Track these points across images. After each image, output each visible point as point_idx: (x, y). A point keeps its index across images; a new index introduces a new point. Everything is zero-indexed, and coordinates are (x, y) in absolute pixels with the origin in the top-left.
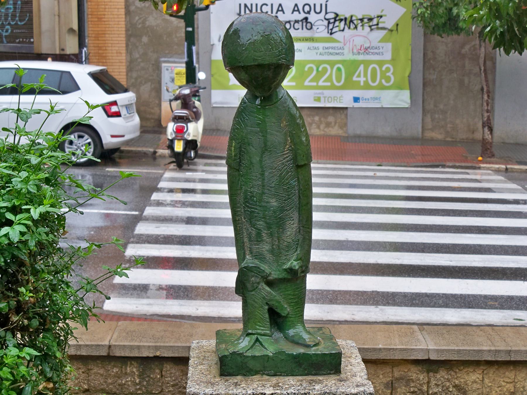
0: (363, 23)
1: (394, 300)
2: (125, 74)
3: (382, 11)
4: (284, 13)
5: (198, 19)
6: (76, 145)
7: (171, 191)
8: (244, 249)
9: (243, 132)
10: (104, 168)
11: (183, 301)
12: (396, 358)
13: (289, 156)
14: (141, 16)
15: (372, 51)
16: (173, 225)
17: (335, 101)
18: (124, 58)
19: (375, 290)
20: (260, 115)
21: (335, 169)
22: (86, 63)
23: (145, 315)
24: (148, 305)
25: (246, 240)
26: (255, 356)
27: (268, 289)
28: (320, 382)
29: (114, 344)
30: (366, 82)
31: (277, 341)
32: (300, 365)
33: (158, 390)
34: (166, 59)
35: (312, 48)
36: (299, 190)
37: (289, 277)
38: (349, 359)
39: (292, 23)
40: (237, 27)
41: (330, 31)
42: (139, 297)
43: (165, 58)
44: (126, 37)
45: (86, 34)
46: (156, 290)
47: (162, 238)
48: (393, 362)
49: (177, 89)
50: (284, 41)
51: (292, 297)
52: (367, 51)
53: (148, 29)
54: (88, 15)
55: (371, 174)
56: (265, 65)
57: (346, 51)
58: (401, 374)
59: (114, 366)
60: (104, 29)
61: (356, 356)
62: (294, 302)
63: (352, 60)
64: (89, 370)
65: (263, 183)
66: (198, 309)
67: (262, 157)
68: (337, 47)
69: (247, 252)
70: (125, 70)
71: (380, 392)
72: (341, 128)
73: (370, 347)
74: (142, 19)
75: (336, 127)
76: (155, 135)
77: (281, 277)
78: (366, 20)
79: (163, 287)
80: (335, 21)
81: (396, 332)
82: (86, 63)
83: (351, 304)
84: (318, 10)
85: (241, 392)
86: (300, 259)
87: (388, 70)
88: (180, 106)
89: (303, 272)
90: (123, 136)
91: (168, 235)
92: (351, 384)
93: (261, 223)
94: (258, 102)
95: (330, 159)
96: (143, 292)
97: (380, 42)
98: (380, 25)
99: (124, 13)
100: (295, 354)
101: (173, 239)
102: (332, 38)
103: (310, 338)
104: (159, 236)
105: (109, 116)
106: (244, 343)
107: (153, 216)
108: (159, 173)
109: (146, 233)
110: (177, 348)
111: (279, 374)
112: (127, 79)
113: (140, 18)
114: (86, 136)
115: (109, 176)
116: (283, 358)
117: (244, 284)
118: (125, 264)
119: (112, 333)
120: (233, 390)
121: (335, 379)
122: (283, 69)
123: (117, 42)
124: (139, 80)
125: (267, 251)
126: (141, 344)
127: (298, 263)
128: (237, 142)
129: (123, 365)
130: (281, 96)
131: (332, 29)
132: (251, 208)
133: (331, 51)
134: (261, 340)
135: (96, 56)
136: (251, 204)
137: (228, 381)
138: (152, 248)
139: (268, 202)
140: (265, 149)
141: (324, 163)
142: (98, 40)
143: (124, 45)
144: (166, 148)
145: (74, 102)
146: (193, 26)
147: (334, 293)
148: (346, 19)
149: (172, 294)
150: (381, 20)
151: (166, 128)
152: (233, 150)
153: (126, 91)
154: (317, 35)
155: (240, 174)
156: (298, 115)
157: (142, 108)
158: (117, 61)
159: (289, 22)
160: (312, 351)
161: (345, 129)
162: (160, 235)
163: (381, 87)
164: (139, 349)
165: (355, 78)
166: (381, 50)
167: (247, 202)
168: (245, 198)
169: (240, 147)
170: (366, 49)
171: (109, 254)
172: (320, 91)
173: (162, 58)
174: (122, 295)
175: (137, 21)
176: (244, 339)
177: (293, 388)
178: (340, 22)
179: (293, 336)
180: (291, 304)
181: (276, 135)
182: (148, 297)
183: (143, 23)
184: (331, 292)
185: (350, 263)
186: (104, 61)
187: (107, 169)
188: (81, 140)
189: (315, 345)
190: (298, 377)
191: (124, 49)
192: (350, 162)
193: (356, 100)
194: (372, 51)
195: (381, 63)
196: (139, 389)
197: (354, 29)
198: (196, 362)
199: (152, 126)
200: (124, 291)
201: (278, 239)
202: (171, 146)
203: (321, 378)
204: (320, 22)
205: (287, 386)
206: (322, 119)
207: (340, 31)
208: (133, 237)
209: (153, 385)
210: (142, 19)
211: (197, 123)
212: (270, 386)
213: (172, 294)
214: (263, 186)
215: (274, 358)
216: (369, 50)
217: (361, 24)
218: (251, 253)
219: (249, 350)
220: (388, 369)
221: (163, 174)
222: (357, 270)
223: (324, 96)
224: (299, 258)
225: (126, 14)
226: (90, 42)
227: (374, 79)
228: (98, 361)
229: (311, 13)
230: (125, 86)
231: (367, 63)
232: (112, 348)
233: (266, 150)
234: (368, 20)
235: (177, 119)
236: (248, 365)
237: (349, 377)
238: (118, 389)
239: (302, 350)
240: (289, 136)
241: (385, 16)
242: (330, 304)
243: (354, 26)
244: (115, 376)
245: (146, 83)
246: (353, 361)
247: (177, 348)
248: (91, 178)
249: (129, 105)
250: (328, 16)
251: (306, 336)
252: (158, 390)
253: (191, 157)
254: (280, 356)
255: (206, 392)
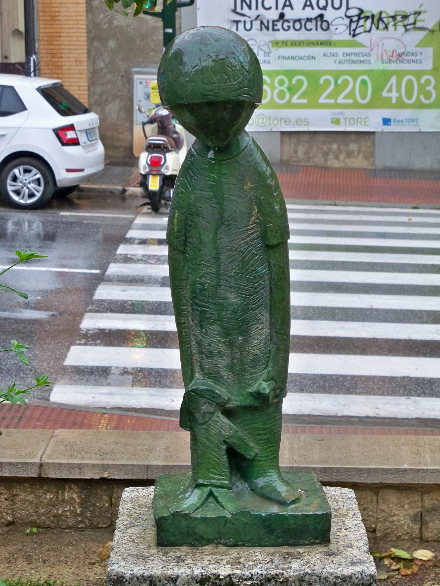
0: (396, 21)
1: (432, 389)
2: (86, 88)
3: (421, 5)
4: (292, 8)
5: (180, 17)
6: (21, 182)
7: (143, 242)
8: (192, 364)
9: (190, 199)
10: (58, 212)
11: (154, 389)
12: (427, 482)
13: (255, 232)
14: (106, 14)
15: (407, 58)
16: (144, 288)
17: (359, 123)
18: (85, 68)
19: (406, 375)
20: (213, 173)
21: (357, 213)
22: (35, 75)
23: (104, 408)
24: (108, 394)
25: (194, 351)
26: (206, 518)
27: (225, 420)
28: (300, 556)
29: (47, 461)
30: (399, 99)
31: (239, 495)
32: (271, 531)
33: (106, 523)
34: (139, 69)
35: (329, 55)
36: (271, 280)
37: (257, 404)
38: (344, 519)
39: (303, 22)
40: (178, 47)
41: (352, 33)
42: (97, 384)
43: (138, 67)
44: (87, 41)
45: (36, 38)
46: (119, 374)
47: (129, 305)
48: (422, 488)
49: (154, 109)
50: (247, 68)
51: (262, 432)
52: (400, 59)
53: (116, 30)
54: (38, 12)
55: (405, 219)
56: (219, 102)
57: (373, 58)
58: (434, 504)
59: (48, 491)
60: (59, 30)
61: (354, 515)
62: (263, 439)
63: (381, 71)
64: (14, 495)
65: (218, 270)
66: (173, 401)
67: (216, 234)
68: (362, 53)
69: (197, 369)
70: (86, 84)
71: (405, 527)
72: (366, 158)
73: (391, 467)
74: (109, 17)
75: (360, 157)
76: (125, 168)
77: (244, 404)
78: (399, 18)
79: (129, 370)
80: (359, 18)
81: (427, 446)
82: (35, 75)
83: (374, 394)
84: (337, 5)
85: (185, 572)
86: (273, 379)
87: (428, 82)
88: (156, 130)
89: (276, 396)
90: (82, 170)
91: (136, 301)
92: (344, 560)
93: (215, 327)
94: (211, 154)
95: (351, 200)
96: (102, 378)
97: (417, 46)
98: (418, 25)
99: (84, 10)
100: (263, 515)
101: (143, 307)
102: (355, 41)
103: (287, 491)
104: (125, 302)
105: (63, 144)
106: (191, 500)
107: (118, 276)
108: (129, 218)
109: (109, 298)
110: (130, 468)
111: (241, 543)
112: (89, 95)
113: (106, 17)
114: (35, 171)
115: (63, 223)
116: (246, 521)
117: (192, 414)
118: (80, 340)
119: (45, 446)
120: (172, 569)
121: (321, 552)
122: (246, 108)
123: (76, 47)
124: (104, 97)
125: (225, 367)
126: (84, 462)
127: (269, 385)
128: (182, 212)
129: (59, 490)
130: (244, 145)
131: (354, 30)
132: (202, 306)
133: (353, 58)
134: (216, 494)
135: (49, 66)
136: (200, 301)
137: (167, 553)
138: (115, 319)
139: (224, 298)
140: (221, 222)
141: (344, 205)
142: (52, 45)
143: (85, 51)
144: (138, 185)
145: (19, 125)
146: (173, 26)
147: (352, 379)
148: (373, 16)
149: (140, 380)
150: (420, 18)
151: (138, 159)
152: (175, 223)
153: (86, 111)
154: (335, 38)
155: (186, 258)
156: (268, 173)
157: (109, 134)
158: (77, 72)
159: (299, 20)
160: (290, 511)
161: (371, 159)
162: (128, 301)
163: (419, 105)
164: (80, 469)
165: (385, 94)
166: (419, 57)
167: (195, 297)
168: (193, 292)
169: (186, 219)
170: (400, 56)
171: (59, 325)
172: (339, 111)
173: (134, 67)
174: (75, 381)
175: (102, 20)
176: (192, 492)
177: (260, 566)
178: (366, 21)
179: (262, 488)
180: (260, 442)
181: (237, 203)
182: (109, 385)
183: (110, 22)
184: (348, 378)
185: (374, 339)
186: (60, 71)
187: (62, 213)
188: (28, 176)
189: (293, 502)
190: (268, 548)
191: (85, 56)
192: (378, 204)
193: (386, 122)
194: (407, 58)
195: (418, 74)
196: (81, 522)
197: (384, 29)
198: (125, 523)
199: (120, 156)
200: (77, 376)
201: (241, 351)
202: (144, 184)
203: (301, 550)
204: (340, 21)
205: (251, 563)
206: (342, 147)
207: (365, 32)
208: (92, 304)
209: (99, 517)
210: (109, 17)
211: (177, 153)
212: (228, 563)
213: (140, 380)
214: (219, 275)
215: (234, 522)
216: (403, 57)
217: (393, 23)
218: (202, 369)
219: (198, 508)
220: (416, 497)
221: (133, 219)
222: (383, 348)
223: (345, 116)
224: (271, 376)
225: (87, 11)
226: (42, 47)
227: (409, 95)
228: (26, 485)
229: (328, 8)
230: (86, 105)
231: (400, 74)
232: (45, 467)
233: (223, 223)
234: (402, 18)
235: (151, 148)
236: (197, 531)
237: (342, 548)
238: (52, 522)
239: (275, 509)
240: (256, 204)
241: (425, 12)
242: (347, 394)
243: (384, 26)
244: (48, 504)
245: (113, 100)
246: (349, 522)
247: (130, 468)
248: (41, 225)
249: (89, 129)
250: (349, 13)
251: (282, 488)
252: (106, 523)
253: (170, 197)
254: (242, 519)
255: (135, 571)
